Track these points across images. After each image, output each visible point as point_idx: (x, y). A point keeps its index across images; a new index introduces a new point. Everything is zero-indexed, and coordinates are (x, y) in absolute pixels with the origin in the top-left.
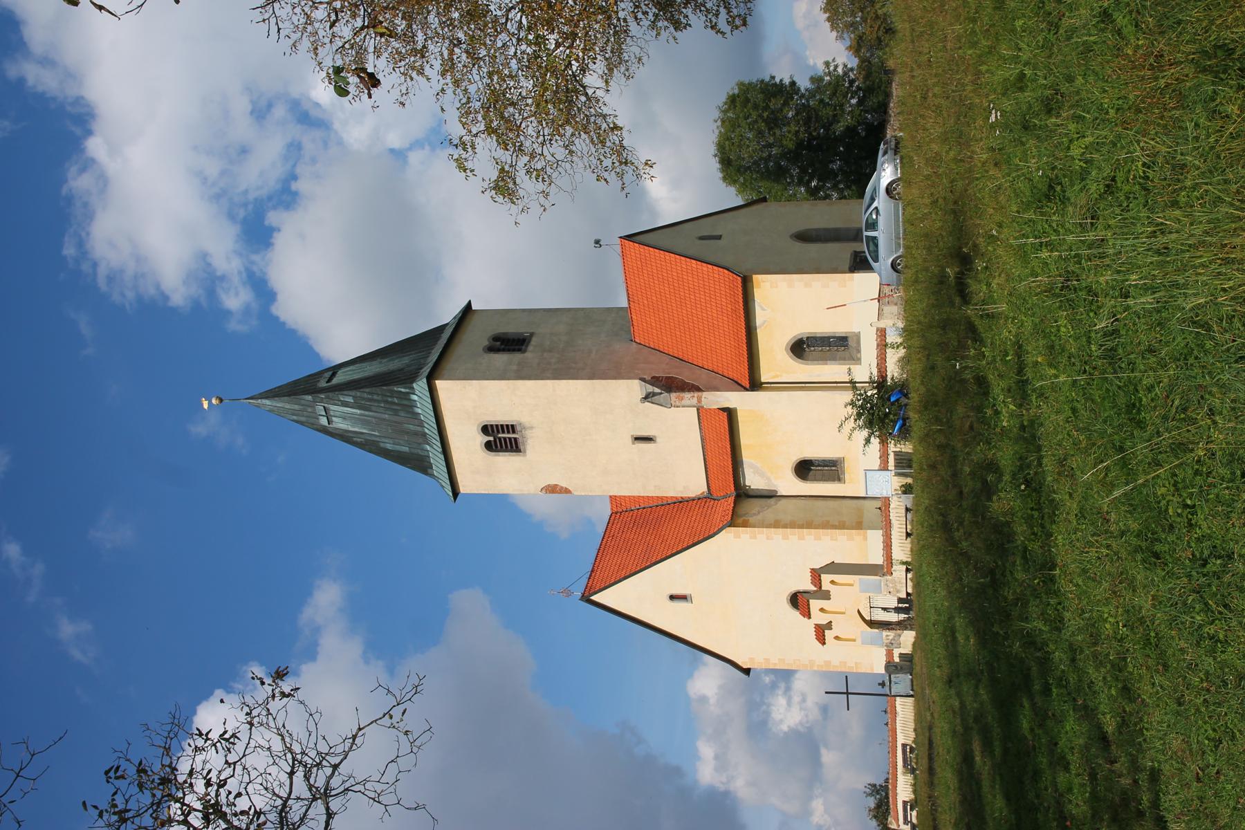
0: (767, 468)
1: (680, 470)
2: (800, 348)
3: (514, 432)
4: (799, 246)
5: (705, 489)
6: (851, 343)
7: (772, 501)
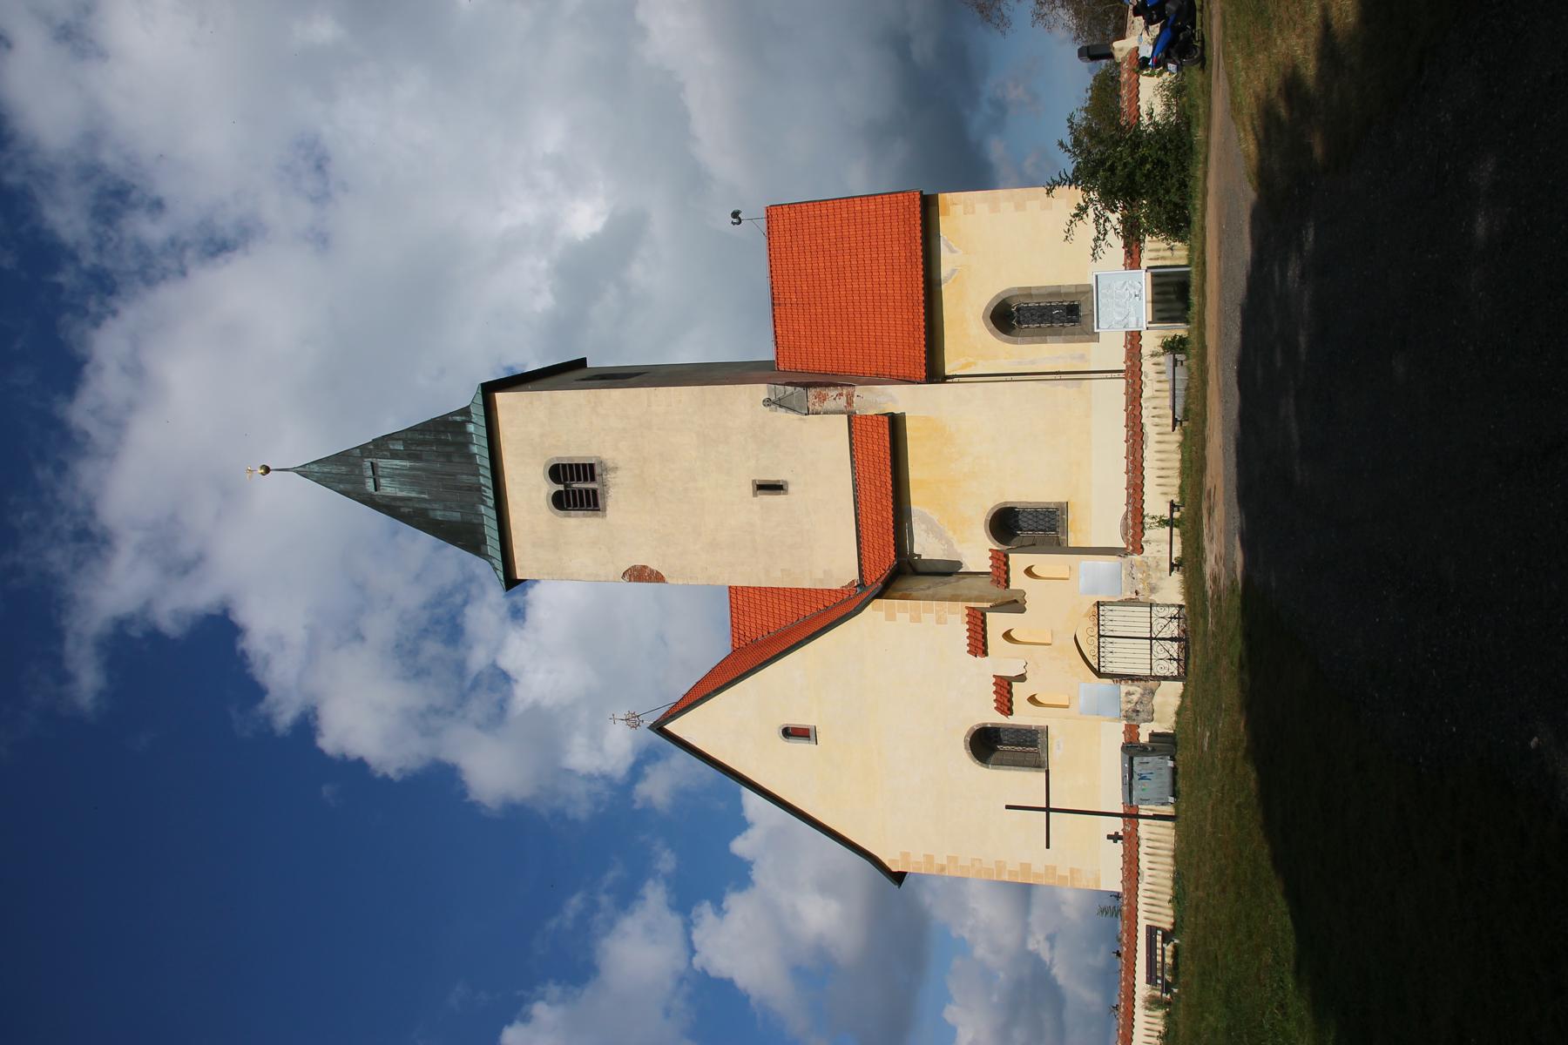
0: (950, 528)
1: (821, 543)
2: (1007, 317)
3: (593, 479)
5: (856, 576)
7: (952, 579)
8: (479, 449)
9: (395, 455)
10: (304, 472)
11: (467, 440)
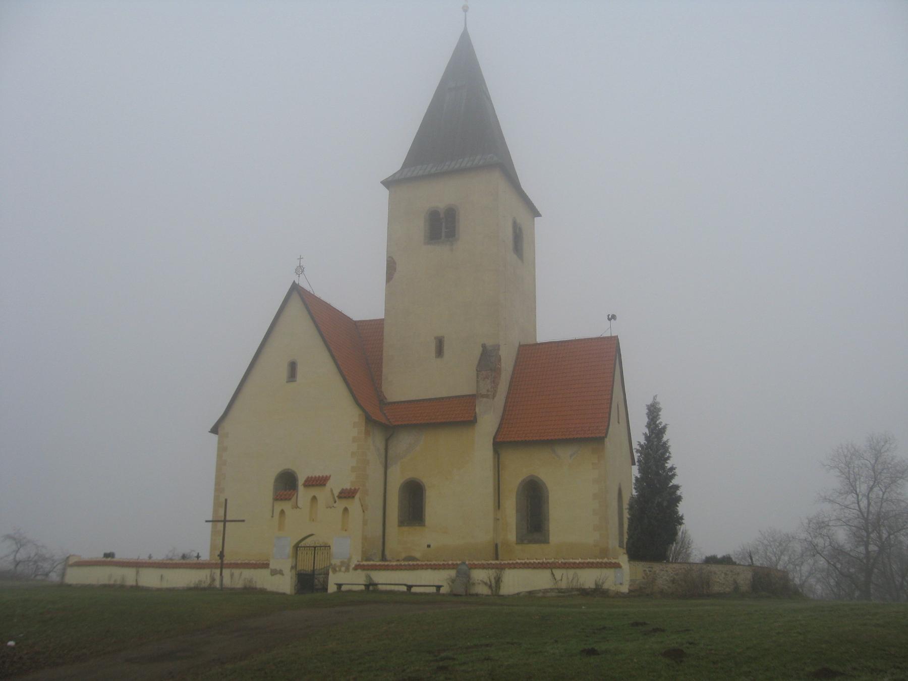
10: (465, 30)
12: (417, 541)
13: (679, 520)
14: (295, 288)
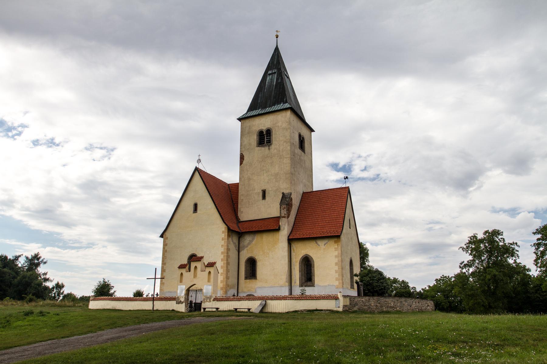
4: (349, 260)
5: (241, 220)
6: (309, 283)
8: (268, 110)
9: (277, 79)
10: (277, 50)
11: (279, 103)
12: (247, 286)
13: (97, 289)
14: (197, 169)
